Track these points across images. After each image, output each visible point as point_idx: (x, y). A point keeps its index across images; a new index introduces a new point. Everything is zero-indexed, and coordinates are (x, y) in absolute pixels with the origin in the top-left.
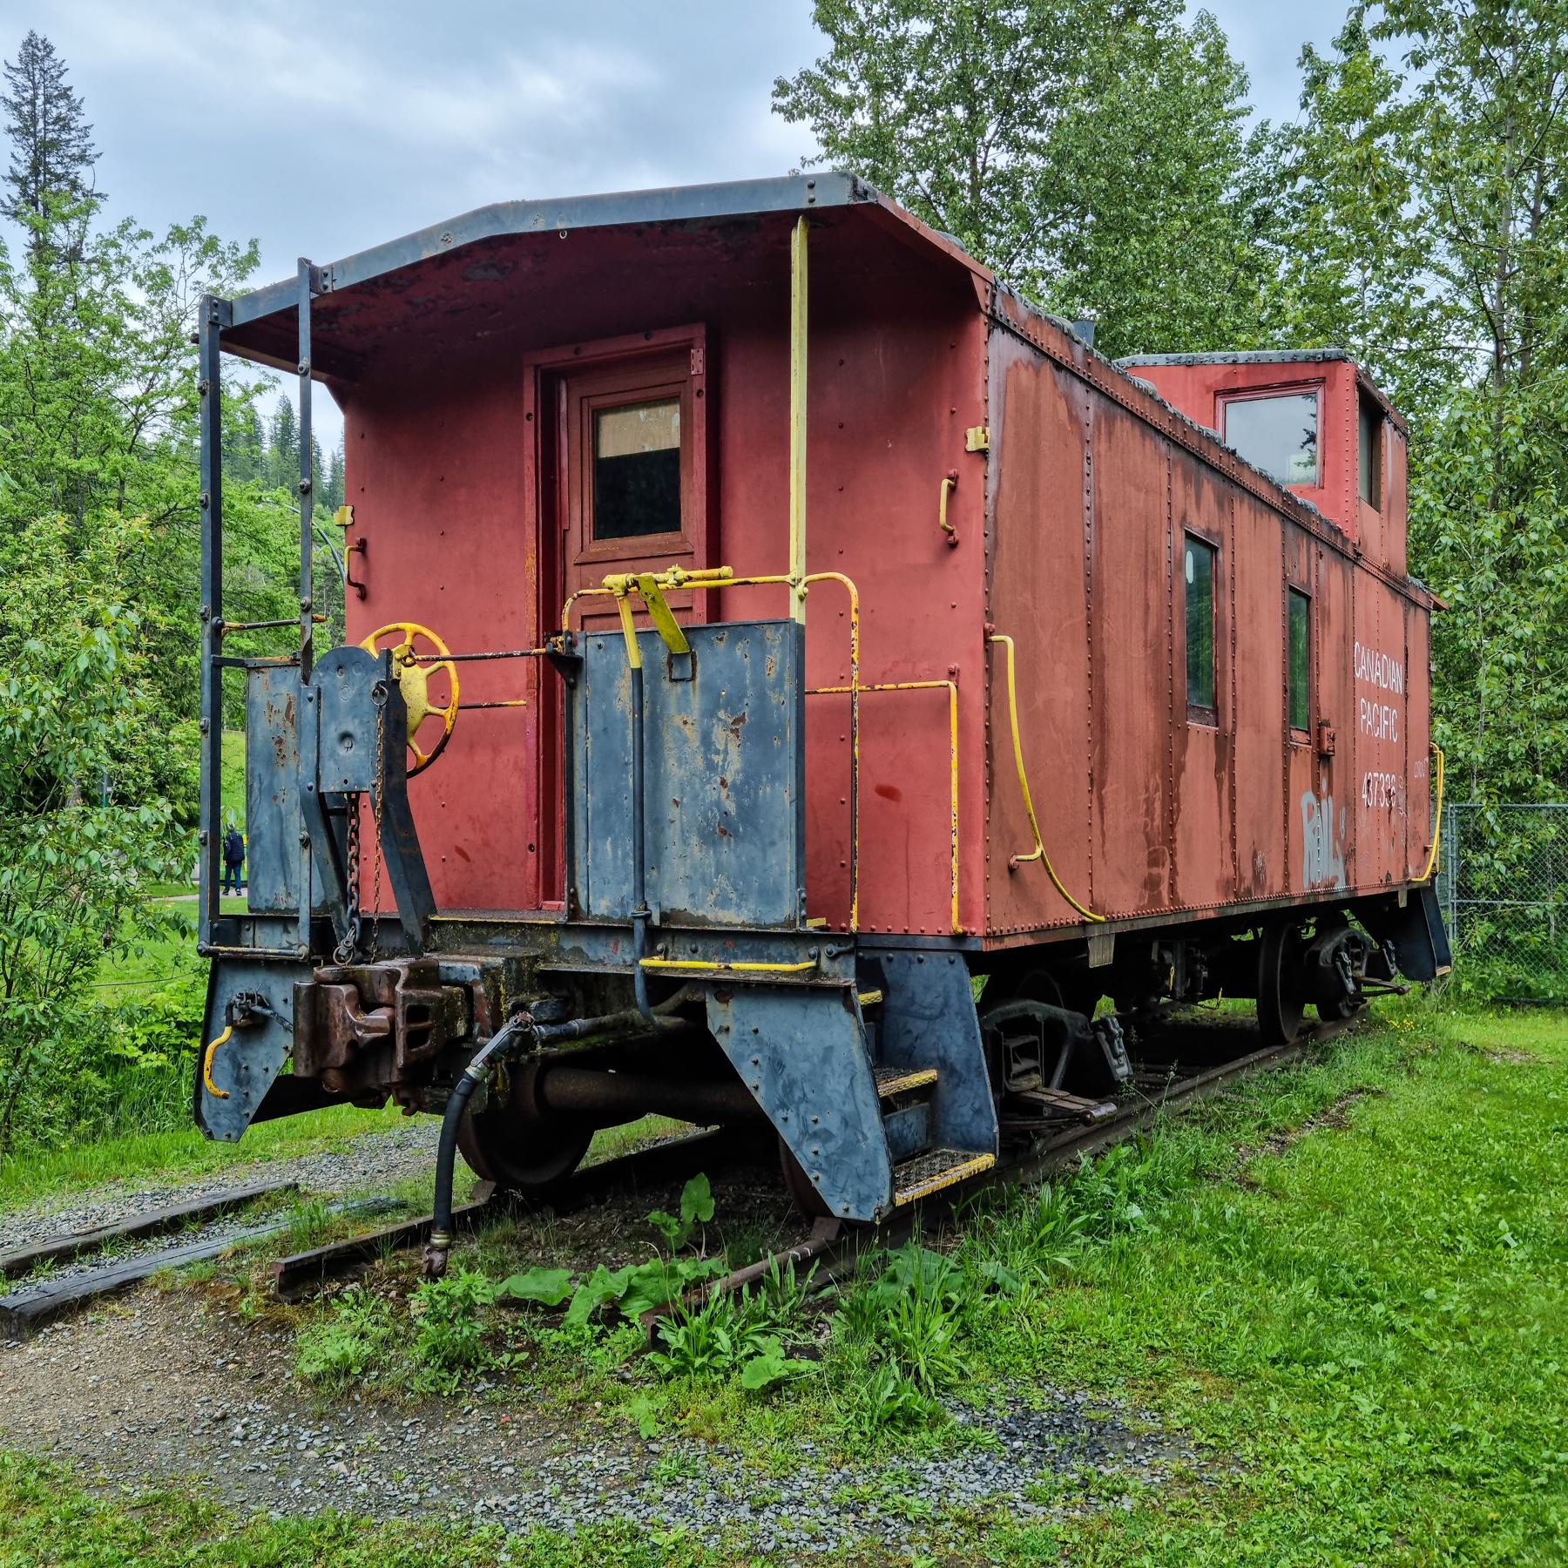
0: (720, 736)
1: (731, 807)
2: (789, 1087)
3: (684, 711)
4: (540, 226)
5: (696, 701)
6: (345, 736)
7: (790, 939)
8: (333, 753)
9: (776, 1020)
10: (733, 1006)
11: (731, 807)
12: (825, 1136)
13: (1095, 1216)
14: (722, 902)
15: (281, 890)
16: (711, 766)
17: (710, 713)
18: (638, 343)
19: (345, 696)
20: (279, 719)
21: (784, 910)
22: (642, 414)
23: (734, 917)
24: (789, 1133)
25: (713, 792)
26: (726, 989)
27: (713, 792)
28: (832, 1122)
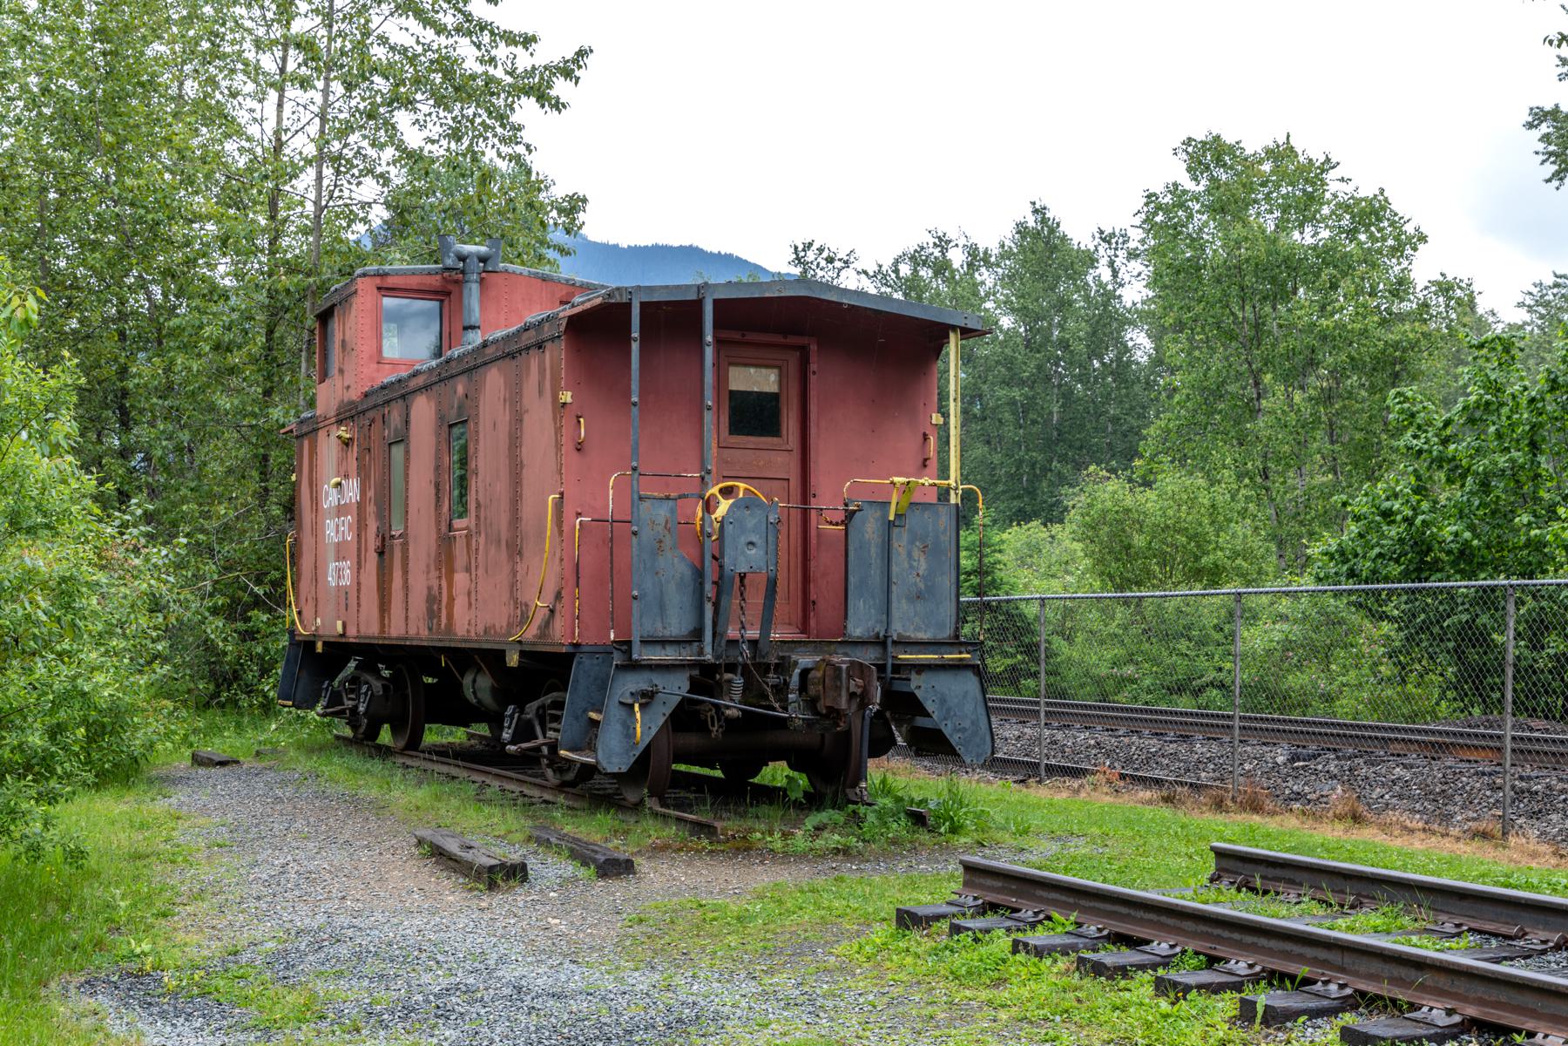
0: (916, 554)
1: (922, 586)
2: (949, 710)
3: (900, 541)
4: (834, 299)
5: (905, 537)
6: (752, 543)
7: (955, 643)
8: (743, 552)
9: (944, 682)
10: (924, 676)
11: (922, 586)
12: (964, 730)
13: (1475, 542)
14: (918, 629)
15: (659, 625)
16: (911, 567)
17: (912, 542)
18: (779, 339)
19: (751, 523)
20: (660, 529)
21: (946, 634)
22: (752, 370)
23: (923, 636)
24: (947, 731)
25: (912, 579)
26: (921, 668)
27: (912, 579)
28: (967, 724)
